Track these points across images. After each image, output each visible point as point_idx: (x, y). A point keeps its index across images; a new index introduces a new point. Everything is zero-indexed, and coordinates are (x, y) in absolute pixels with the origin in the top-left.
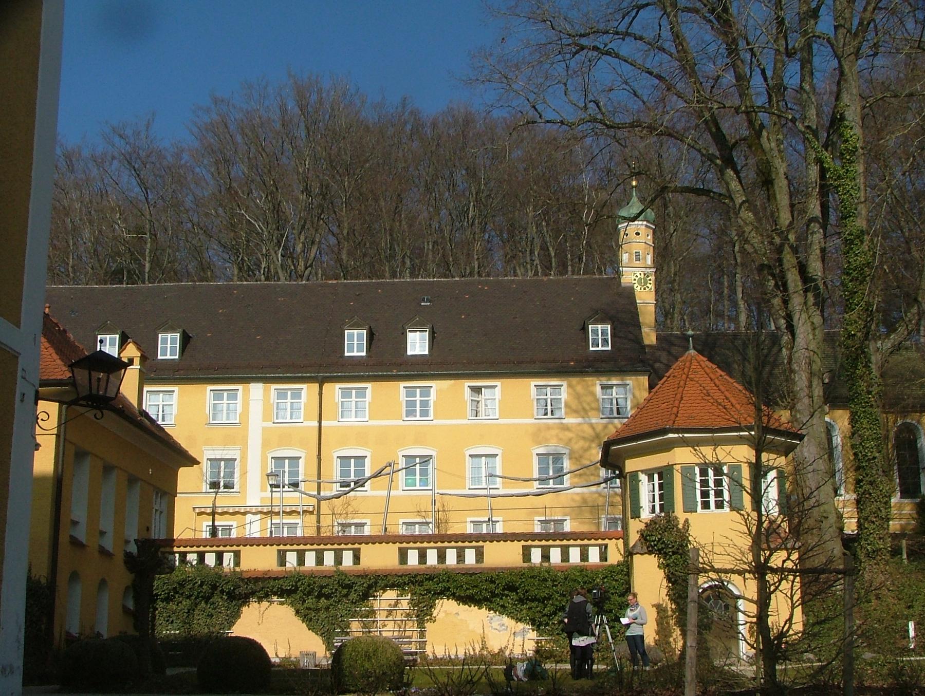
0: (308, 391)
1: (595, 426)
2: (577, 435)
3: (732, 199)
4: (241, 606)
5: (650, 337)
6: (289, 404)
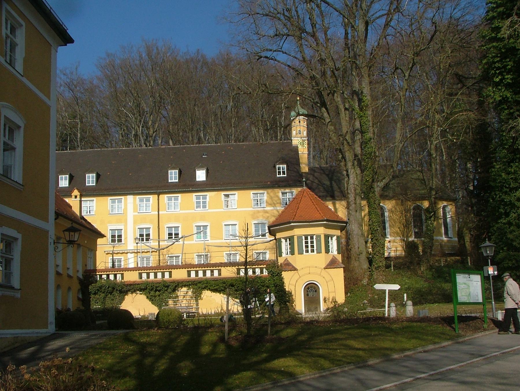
0: (153, 198)
1: (279, 211)
2: (271, 215)
3: (325, 120)
4: (124, 296)
5: (305, 168)
6: (145, 204)
